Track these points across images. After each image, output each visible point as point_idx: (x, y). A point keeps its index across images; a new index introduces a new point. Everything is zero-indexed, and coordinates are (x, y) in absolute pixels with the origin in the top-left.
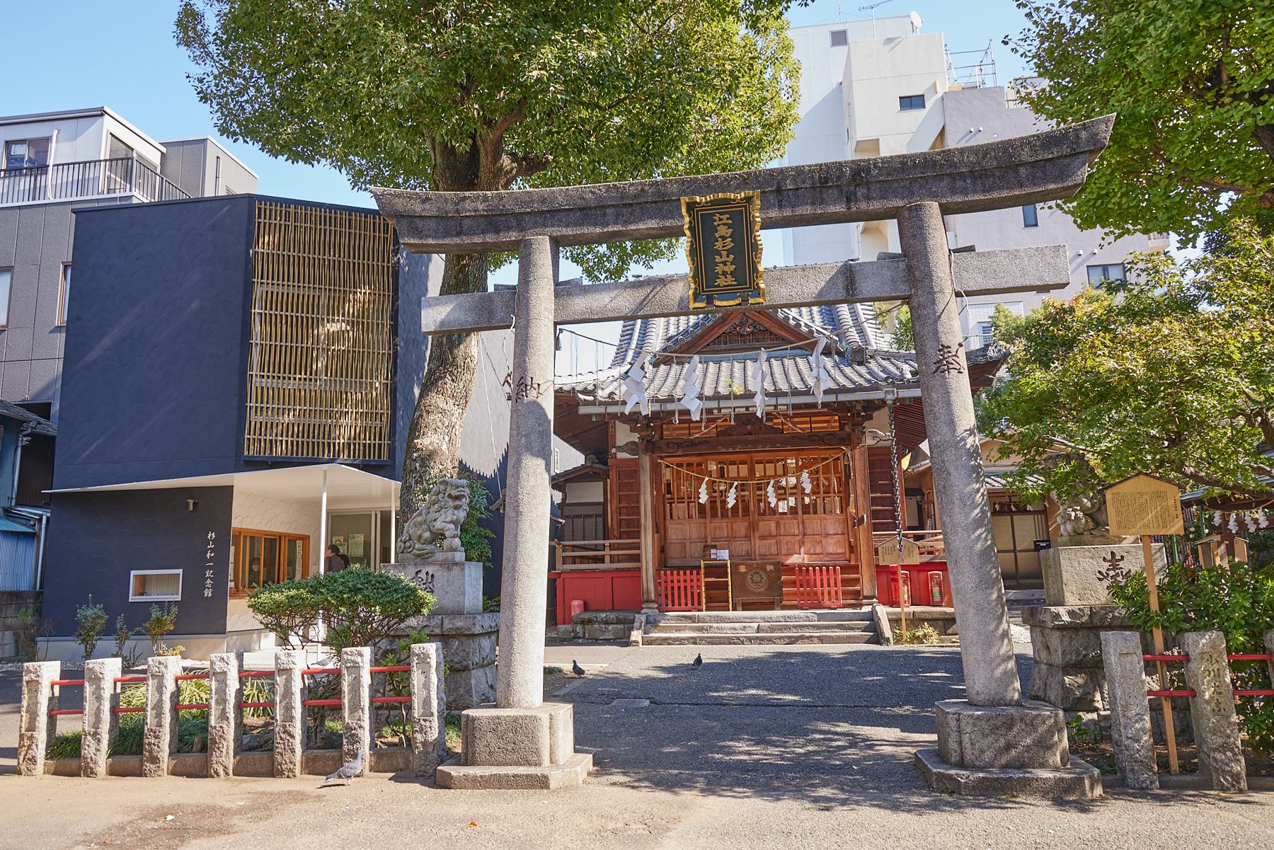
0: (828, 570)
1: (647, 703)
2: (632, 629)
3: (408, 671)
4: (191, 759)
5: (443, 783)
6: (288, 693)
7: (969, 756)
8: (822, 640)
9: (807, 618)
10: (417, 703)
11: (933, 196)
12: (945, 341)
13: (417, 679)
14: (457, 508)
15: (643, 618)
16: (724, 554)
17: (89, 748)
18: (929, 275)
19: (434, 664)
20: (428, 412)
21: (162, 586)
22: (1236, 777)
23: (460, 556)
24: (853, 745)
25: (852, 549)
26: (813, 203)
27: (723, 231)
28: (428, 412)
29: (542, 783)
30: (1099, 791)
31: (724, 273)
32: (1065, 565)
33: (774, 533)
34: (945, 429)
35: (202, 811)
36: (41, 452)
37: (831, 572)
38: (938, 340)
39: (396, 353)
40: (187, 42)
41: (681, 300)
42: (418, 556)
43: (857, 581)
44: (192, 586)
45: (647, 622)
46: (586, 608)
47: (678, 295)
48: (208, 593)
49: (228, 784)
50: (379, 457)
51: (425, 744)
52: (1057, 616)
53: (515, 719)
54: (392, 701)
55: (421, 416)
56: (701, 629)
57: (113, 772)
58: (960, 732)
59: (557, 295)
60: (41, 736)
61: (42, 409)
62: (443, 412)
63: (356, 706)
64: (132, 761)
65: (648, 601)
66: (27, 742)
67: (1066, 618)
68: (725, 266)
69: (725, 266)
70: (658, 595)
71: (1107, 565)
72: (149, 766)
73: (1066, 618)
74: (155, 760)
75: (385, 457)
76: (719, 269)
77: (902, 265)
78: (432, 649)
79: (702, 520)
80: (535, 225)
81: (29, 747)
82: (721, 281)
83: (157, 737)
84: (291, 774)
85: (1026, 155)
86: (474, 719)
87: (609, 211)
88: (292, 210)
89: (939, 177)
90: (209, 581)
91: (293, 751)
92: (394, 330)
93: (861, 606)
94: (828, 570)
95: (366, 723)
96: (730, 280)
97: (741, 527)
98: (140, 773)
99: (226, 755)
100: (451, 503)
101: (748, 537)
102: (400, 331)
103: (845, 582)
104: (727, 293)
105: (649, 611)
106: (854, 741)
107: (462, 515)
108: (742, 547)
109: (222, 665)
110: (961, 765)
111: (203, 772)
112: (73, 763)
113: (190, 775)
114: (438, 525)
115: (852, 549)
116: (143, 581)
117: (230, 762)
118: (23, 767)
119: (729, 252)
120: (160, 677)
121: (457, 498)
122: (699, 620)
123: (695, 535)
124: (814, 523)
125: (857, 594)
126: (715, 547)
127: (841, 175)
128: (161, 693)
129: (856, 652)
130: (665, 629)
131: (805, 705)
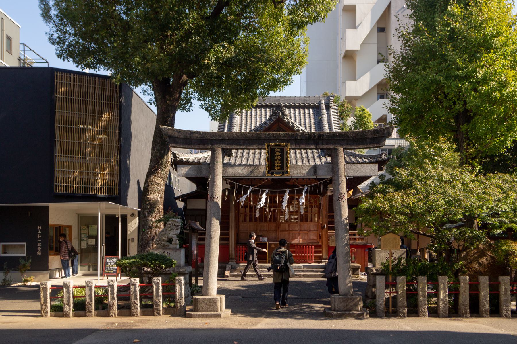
0: (309, 247)
1: (241, 297)
2: (225, 270)
3: (174, 286)
5: (190, 316)
6: (135, 291)
7: (336, 308)
8: (304, 276)
9: (299, 267)
10: (178, 294)
11: (341, 145)
12: (341, 191)
13: (178, 287)
14: (177, 229)
15: (230, 266)
17: (66, 308)
18: (338, 171)
19: (183, 283)
20: (151, 184)
22: (404, 314)
23: (178, 246)
24: (308, 308)
25: (320, 237)
26: (306, 144)
27: (278, 153)
28: (151, 184)
29: (219, 316)
30: (368, 316)
31: (277, 166)
32: (377, 255)
33: (287, 229)
34: (339, 218)
37: (310, 248)
38: (339, 190)
39: (121, 145)
41: (264, 172)
42: (164, 246)
43: (320, 252)
44: (31, 250)
45: (232, 268)
47: (263, 170)
48: (39, 253)
49: (117, 319)
50: (114, 194)
51: (180, 306)
52: (372, 271)
53: (210, 299)
54: (169, 293)
55: (148, 186)
57: (75, 316)
58: (335, 302)
59: (223, 167)
60: (49, 305)
62: (158, 184)
63: (158, 295)
64: (82, 312)
65: (232, 259)
66: (44, 307)
67: (375, 271)
68: (278, 164)
69: (278, 164)
70: (236, 256)
71: (389, 255)
72: (88, 314)
73: (375, 271)
74: (90, 312)
75: (117, 193)
76: (276, 165)
77: (331, 166)
78: (182, 278)
79: (255, 223)
80: (217, 144)
81: (45, 308)
82: (276, 168)
83: (90, 305)
84: (137, 316)
85: (369, 136)
86: (197, 299)
87: (241, 141)
88: (72, 75)
90: (39, 248)
91: (137, 309)
92: (120, 135)
93: (321, 262)
94: (309, 247)
95: (161, 301)
96: (279, 168)
97: (273, 226)
98: (85, 316)
99: (115, 310)
100: (175, 228)
101: (276, 231)
102: (122, 135)
103: (316, 252)
104: (278, 172)
105: (232, 263)
106: (308, 307)
107: (178, 232)
108: (273, 235)
109: (112, 283)
110: (334, 310)
111: (108, 315)
112: (61, 313)
113: (102, 316)
114: (171, 235)
115: (320, 237)
117: (116, 312)
118: (43, 315)
119: (279, 160)
121: (177, 226)
124: (305, 225)
125: (320, 258)
126: (261, 236)
127: (315, 136)
128: (91, 291)
129: (317, 281)
131: (295, 298)
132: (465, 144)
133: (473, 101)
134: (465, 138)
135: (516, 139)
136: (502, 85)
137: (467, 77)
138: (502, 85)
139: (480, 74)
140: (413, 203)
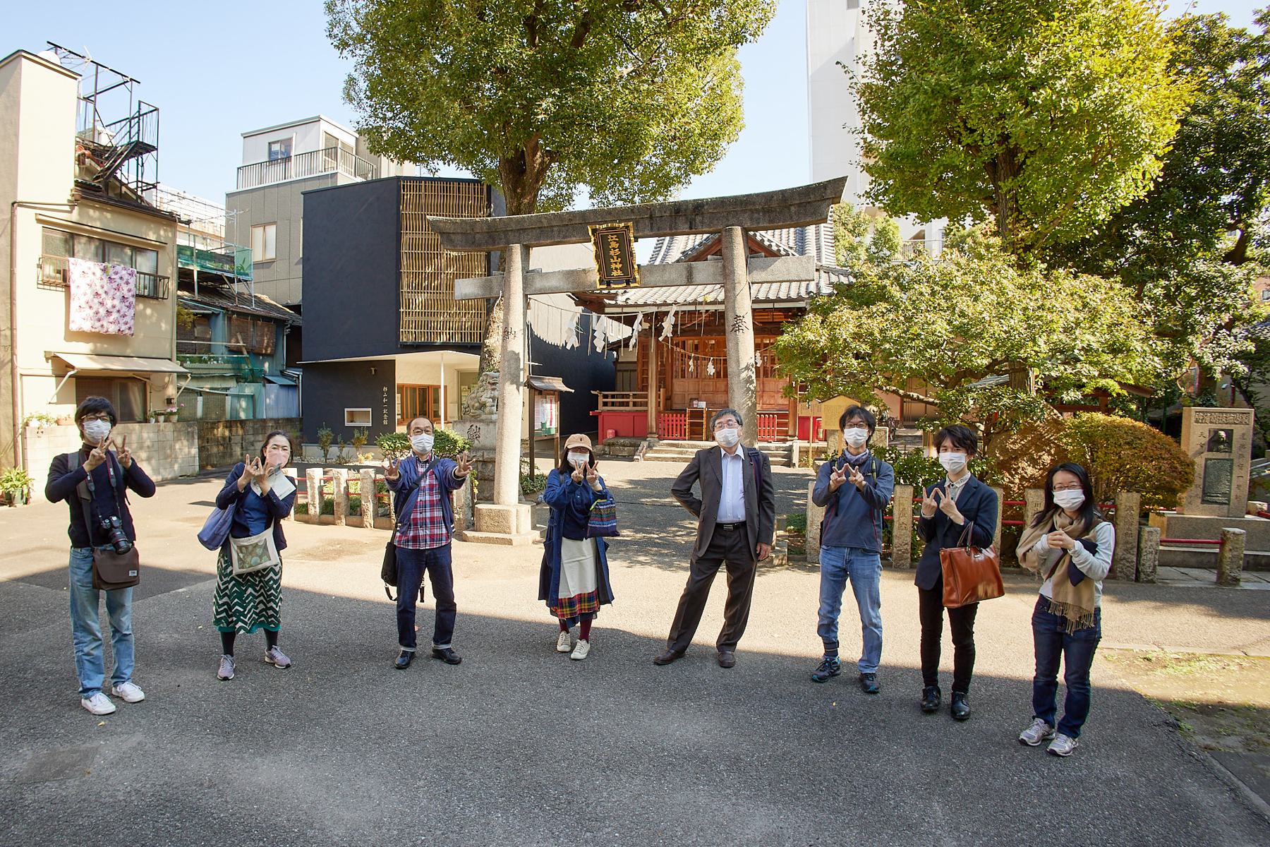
4: (354, 519)
16: (703, 405)
18: (733, 272)
21: (361, 418)
27: (614, 245)
29: (510, 542)
35: (353, 543)
36: (296, 335)
40: (351, 100)
43: (786, 425)
44: (377, 418)
46: (616, 434)
48: (385, 422)
56: (681, 453)
61: (297, 308)
64: (330, 517)
68: (616, 265)
69: (616, 265)
76: (613, 266)
82: (615, 273)
89: (744, 211)
96: (619, 273)
99: (369, 518)
103: (779, 425)
114: (483, 399)
116: (351, 414)
120: (338, 479)
122: (682, 446)
123: (691, 389)
130: (657, 451)
132: (1010, 220)
133: (1019, 124)
134: (1011, 209)
135: (1226, 846)
136: (1085, 85)
137: (1004, 76)
138: (1085, 85)
139: (1035, 65)
140: (881, 331)
